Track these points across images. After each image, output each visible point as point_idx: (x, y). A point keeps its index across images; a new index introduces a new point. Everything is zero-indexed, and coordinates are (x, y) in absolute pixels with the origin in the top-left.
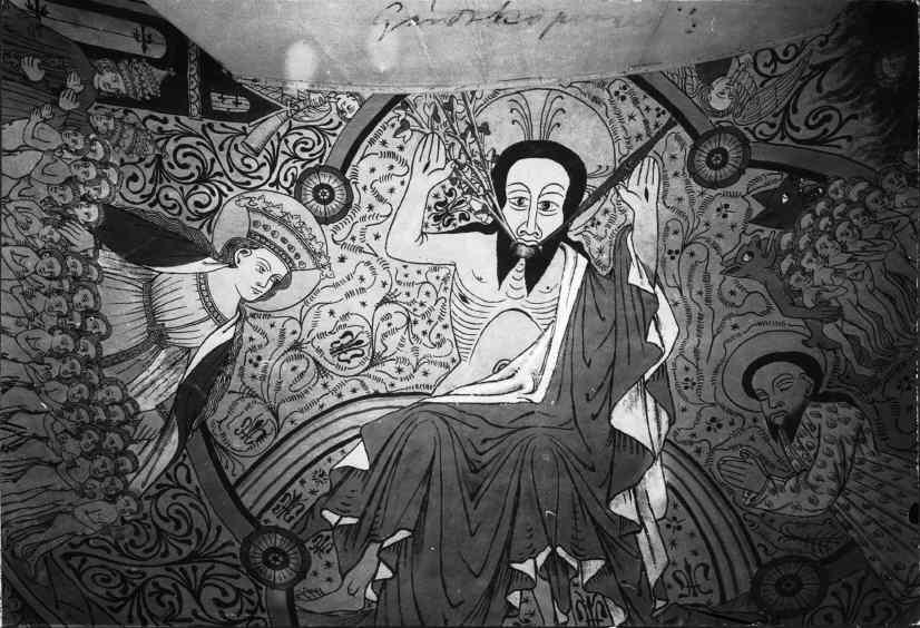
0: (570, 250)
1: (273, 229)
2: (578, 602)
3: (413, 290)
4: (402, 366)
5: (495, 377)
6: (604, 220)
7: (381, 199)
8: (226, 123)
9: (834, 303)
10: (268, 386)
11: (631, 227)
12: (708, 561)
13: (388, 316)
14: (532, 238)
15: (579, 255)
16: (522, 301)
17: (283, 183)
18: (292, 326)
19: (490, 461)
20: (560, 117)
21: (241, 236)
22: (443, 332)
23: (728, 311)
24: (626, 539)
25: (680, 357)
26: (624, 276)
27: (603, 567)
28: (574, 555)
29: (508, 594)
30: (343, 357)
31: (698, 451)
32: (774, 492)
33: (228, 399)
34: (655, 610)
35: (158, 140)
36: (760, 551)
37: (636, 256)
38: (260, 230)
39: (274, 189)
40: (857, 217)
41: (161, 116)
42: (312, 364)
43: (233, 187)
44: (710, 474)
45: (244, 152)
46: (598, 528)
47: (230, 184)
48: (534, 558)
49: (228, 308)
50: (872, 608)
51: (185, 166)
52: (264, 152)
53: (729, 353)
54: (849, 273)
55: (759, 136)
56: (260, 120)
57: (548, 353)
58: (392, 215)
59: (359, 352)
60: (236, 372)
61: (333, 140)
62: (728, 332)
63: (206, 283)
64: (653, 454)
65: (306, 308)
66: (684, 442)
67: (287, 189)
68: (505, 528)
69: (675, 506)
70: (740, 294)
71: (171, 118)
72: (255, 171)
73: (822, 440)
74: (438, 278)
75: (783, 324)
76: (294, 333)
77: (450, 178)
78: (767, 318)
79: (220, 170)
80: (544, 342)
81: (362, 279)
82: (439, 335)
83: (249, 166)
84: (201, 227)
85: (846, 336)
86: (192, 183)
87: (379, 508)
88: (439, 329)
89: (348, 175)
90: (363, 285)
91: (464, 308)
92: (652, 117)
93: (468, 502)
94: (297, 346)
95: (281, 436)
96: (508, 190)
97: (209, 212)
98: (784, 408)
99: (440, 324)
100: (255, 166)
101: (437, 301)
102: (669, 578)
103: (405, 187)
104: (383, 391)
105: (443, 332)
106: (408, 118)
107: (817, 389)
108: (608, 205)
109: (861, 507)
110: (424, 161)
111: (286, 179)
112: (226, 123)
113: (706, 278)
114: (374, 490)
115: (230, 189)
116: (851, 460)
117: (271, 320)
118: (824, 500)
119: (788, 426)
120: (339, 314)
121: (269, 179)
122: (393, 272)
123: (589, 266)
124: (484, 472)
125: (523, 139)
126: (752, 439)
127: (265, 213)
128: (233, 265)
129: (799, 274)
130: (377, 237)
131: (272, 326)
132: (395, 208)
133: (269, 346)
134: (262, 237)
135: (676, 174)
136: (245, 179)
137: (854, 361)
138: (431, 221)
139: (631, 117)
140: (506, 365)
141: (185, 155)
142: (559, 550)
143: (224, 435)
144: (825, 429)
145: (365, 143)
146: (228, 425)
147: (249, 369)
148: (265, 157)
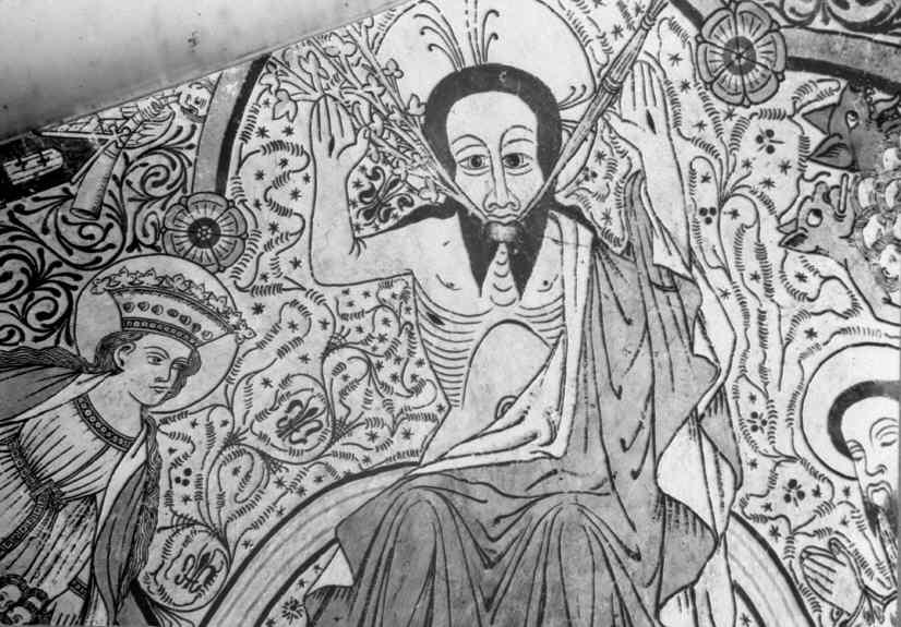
0: (563, 219)
1: (152, 304)
3: (364, 322)
4: (375, 430)
5: (498, 425)
6: (601, 169)
7: (285, 212)
8: (40, 195)
10: (208, 504)
13: (340, 367)
14: (508, 210)
15: (579, 226)
16: (515, 308)
17: (143, 240)
19: (508, 549)
25: (742, 380)
30: (296, 436)
31: (775, 532)
33: (160, 539)
37: (658, 219)
38: (137, 313)
39: (136, 252)
42: (257, 458)
44: (788, 570)
45: (79, 220)
49: (128, 426)
52: (105, 210)
53: (807, 377)
55: (792, 16)
58: (307, 225)
59: (315, 425)
60: (162, 500)
61: (191, 155)
62: (801, 343)
63: (89, 405)
65: (231, 387)
66: (756, 518)
67: (152, 246)
70: (814, 281)
72: (103, 239)
74: (394, 296)
76: (225, 423)
78: (852, 322)
80: (552, 375)
81: (293, 326)
82: (414, 377)
83: (91, 237)
84: (57, 341)
88: (412, 369)
89: (228, 195)
90: (298, 334)
91: (440, 333)
93: (483, 612)
94: (233, 439)
95: (234, 568)
96: (454, 149)
99: (413, 360)
100: (98, 233)
103: (311, 184)
104: (355, 470)
106: (283, 86)
108: (600, 146)
110: (326, 139)
111: (146, 235)
113: (761, 252)
114: (364, 614)
117: (191, 418)
120: (276, 381)
122: (332, 304)
124: (500, 566)
125: (452, 70)
126: (844, 523)
127: (137, 288)
128: (116, 371)
130: (296, 264)
134: (141, 320)
135: (685, 86)
136: (93, 256)
138: (362, 220)
140: (510, 405)
143: (162, 590)
145: (237, 142)
146: (165, 575)
147: (179, 490)
148: (109, 216)
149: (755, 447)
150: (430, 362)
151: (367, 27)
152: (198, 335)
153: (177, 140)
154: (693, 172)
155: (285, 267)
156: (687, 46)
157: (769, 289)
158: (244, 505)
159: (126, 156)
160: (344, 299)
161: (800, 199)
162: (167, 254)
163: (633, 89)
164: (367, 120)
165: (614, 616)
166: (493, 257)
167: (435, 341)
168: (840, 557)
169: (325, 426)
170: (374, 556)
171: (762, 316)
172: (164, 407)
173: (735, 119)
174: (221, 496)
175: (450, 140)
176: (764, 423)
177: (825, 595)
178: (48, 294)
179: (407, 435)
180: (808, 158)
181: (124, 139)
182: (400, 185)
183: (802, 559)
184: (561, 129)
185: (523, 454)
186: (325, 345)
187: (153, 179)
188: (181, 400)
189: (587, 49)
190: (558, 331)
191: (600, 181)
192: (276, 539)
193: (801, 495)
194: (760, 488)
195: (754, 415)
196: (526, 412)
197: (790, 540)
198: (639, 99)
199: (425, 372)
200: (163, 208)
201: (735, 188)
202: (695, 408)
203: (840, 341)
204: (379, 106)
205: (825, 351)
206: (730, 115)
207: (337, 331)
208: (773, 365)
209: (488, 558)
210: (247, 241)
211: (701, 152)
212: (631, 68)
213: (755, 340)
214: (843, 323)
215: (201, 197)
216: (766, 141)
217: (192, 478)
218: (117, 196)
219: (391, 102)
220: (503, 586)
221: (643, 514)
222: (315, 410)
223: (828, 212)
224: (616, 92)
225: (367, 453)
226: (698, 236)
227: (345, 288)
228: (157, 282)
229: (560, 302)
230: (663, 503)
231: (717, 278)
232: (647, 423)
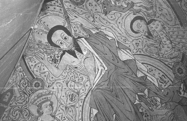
0: (79, 40)
2: (150, 102)
5: (96, 73)
6: (76, 29)
7: (45, 73)
8: (11, 100)
9: (130, 2)
10: (71, 119)
11: (82, 25)
12: (163, 74)
16: (84, 57)
17: (30, 93)
18: (61, 106)
20: (46, 24)
21: (37, 108)
22: (81, 76)
26: (92, 33)
28: (142, 92)
29: (139, 111)
30: (73, 100)
31: (140, 52)
34: (163, 93)
35: (8, 119)
36: (169, 65)
37: (89, 28)
38: (38, 103)
41: (3, 116)
42: (71, 107)
43: (26, 105)
44: (146, 55)
45: (19, 99)
47: (25, 106)
48: (136, 99)
51: (17, 114)
52: (22, 94)
56: (14, 91)
59: (75, 96)
61: (26, 77)
64: (134, 60)
67: (32, 93)
68: (127, 99)
69: (147, 66)
70: (113, 16)
71: (5, 113)
72: (25, 98)
73: (158, 33)
76: (63, 107)
77: (47, 55)
79: (21, 106)
80: (96, 59)
82: (81, 77)
83: (23, 99)
84: (31, 117)
85: (139, 6)
86: (21, 114)
87: (107, 115)
88: (79, 77)
89: (35, 77)
92: (57, 4)
94: (66, 108)
96: (57, 44)
97: (29, 113)
98: (145, 31)
99: (79, 76)
101: (73, 73)
104: (85, 96)
105: (81, 76)
106: (29, 57)
107: (146, 21)
110: (41, 59)
111: (30, 92)
112: (11, 100)
113: (104, 19)
115: (26, 106)
117: (58, 110)
120: (64, 95)
121: (28, 96)
122: (62, 78)
123: (85, 38)
126: (146, 42)
127: (35, 100)
130: (52, 78)
131: (59, 111)
132: (48, 70)
133: (63, 114)
134: (40, 104)
135: (75, 8)
136: (26, 101)
137: (146, 11)
139: (55, 8)
141: (14, 114)
142: (138, 94)
144: (156, 30)
145: (30, 70)
149: (128, 44)
150: (81, 74)
151: (32, 40)
152: (49, 99)
153: (22, 77)
155: (51, 80)
158: (75, 115)
159: (18, 85)
160: (63, 76)
162: (35, 92)
163: (70, 15)
164: (43, 51)
165: (132, 82)
166: (75, 53)
167: (79, 70)
169: (76, 95)
170: (97, 105)
171: (112, 27)
172: (53, 112)
173: (84, 6)
174: (71, 116)
175: (55, 43)
176: (126, 40)
177: (153, 53)
178: (24, 112)
179: (87, 86)
180: (97, 1)
181: (15, 83)
182: (55, 55)
183: (146, 51)
184: (67, 29)
185: (103, 73)
186: (66, 84)
187: (24, 84)
188: (55, 109)
189: (60, 16)
191: (78, 30)
192: (83, 115)
193: (138, 44)
194: (133, 48)
196: (98, 68)
197: (142, 50)
198: (71, 15)
199: (81, 76)
200: (29, 87)
201: (93, 14)
202: (117, 47)
203: (123, 20)
204: (43, 48)
205: (123, 23)
206: (83, 6)
207: (66, 81)
208: (120, 32)
209: (111, 91)
210: (43, 81)
211: (85, 14)
212: (67, 13)
213: (115, 31)
214: (122, 17)
215: (32, 81)
217: (65, 118)
218: (22, 91)
219: (44, 46)
220: (116, 93)
221: (123, 66)
222: (73, 94)
223: (106, 6)
224: (68, 17)
225: (84, 93)
226: (95, 25)
227: (61, 75)
228: (37, 97)
229: (88, 50)
231: (103, 28)
232: (114, 55)
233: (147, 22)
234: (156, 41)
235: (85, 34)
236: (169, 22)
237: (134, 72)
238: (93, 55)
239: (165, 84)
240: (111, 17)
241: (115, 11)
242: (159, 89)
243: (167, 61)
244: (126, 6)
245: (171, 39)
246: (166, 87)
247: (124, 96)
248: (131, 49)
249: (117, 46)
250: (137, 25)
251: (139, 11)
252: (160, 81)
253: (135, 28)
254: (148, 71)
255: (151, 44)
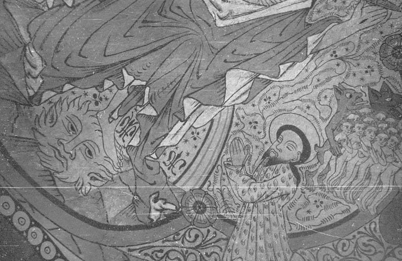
2: (129, 117)
9: (343, 150)
11: (340, 22)
23: (315, 99)
24: (174, 117)
26: (311, 34)
27: (154, 116)
28: (150, 98)
29: (107, 79)
31: (237, 124)
32: (238, 172)
34: (150, 156)
36: (207, 183)
40: (392, 141)
44: (229, 136)
46: (171, 100)
48: (135, 79)
50: (212, 253)
54: (361, 150)
57: (245, 14)
62: (305, 105)
66: (237, 114)
68: (137, 53)
69: (204, 130)
70: (326, 102)
75: (321, 130)
80: (252, 7)
85: (329, 164)
98: (279, 153)
102: (168, 152)
107: (298, 163)
109: (253, 216)
113: (328, 79)
116: (272, 199)
118: (247, 198)
119: (271, 160)
123: (307, 9)
126: (257, 147)
129: (350, 125)
142: (147, 89)
144: (279, 178)
149: (260, 103)
154: (348, 43)
156: (398, 30)
157: (316, 86)
161: (353, 88)
168: (246, 151)
171: (306, 87)
180: (369, 87)
183: (235, 138)
185: (211, 8)
190: (266, 4)
194: (247, 111)
195: (270, 98)
201: (348, 62)
202: (260, 74)
211: (357, 45)
213: (295, 88)
216: (369, 70)
223: (353, 99)
226: (324, 54)
230: (222, 77)
231: (312, 65)
233: (296, 166)
234: (256, 170)
235: (316, 16)
236: (293, 210)
237: (196, 92)
238: (263, 5)
239: (167, 164)
240: (326, 97)
241: (335, 110)
242: (157, 147)
243: (215, 181)
244: (338, 139)
245: (260, 205)
246: (162, 165)
247: (143, 43)
248: (247, 105)
249: (260, 76)
250: (294, 142)
251: (321, 159)
252: (173, 153)
253: (288, 135)
254: (195, 128)
255: (251, 156)
